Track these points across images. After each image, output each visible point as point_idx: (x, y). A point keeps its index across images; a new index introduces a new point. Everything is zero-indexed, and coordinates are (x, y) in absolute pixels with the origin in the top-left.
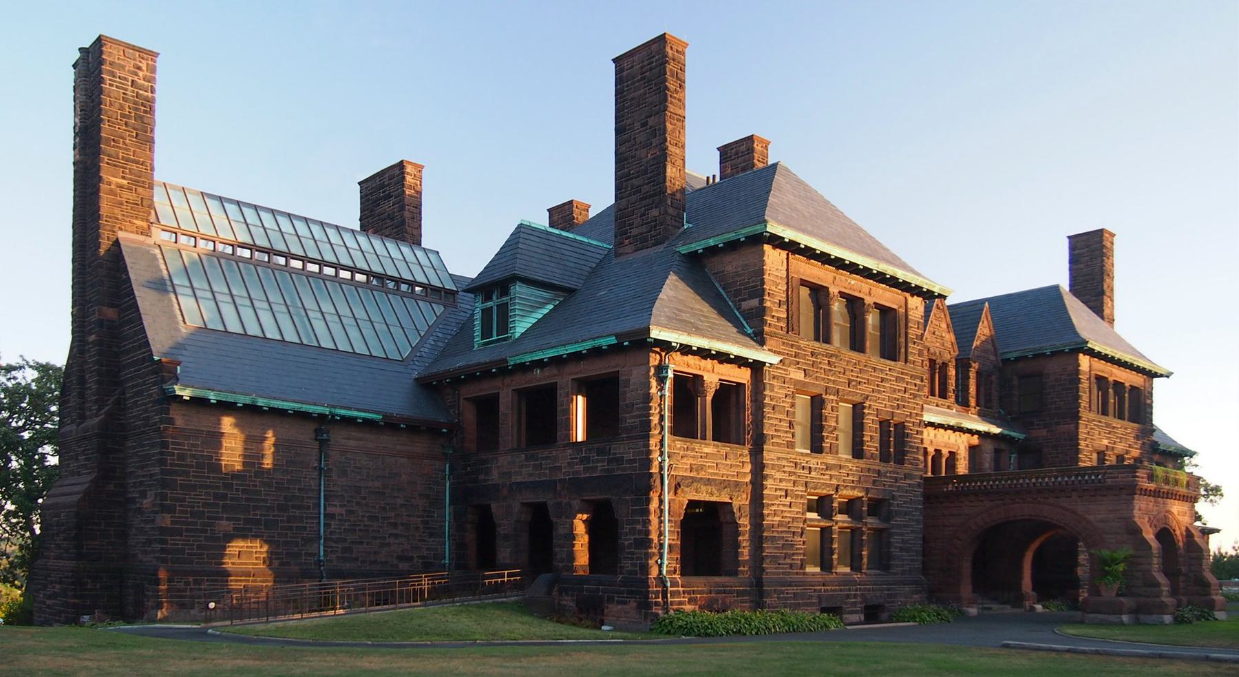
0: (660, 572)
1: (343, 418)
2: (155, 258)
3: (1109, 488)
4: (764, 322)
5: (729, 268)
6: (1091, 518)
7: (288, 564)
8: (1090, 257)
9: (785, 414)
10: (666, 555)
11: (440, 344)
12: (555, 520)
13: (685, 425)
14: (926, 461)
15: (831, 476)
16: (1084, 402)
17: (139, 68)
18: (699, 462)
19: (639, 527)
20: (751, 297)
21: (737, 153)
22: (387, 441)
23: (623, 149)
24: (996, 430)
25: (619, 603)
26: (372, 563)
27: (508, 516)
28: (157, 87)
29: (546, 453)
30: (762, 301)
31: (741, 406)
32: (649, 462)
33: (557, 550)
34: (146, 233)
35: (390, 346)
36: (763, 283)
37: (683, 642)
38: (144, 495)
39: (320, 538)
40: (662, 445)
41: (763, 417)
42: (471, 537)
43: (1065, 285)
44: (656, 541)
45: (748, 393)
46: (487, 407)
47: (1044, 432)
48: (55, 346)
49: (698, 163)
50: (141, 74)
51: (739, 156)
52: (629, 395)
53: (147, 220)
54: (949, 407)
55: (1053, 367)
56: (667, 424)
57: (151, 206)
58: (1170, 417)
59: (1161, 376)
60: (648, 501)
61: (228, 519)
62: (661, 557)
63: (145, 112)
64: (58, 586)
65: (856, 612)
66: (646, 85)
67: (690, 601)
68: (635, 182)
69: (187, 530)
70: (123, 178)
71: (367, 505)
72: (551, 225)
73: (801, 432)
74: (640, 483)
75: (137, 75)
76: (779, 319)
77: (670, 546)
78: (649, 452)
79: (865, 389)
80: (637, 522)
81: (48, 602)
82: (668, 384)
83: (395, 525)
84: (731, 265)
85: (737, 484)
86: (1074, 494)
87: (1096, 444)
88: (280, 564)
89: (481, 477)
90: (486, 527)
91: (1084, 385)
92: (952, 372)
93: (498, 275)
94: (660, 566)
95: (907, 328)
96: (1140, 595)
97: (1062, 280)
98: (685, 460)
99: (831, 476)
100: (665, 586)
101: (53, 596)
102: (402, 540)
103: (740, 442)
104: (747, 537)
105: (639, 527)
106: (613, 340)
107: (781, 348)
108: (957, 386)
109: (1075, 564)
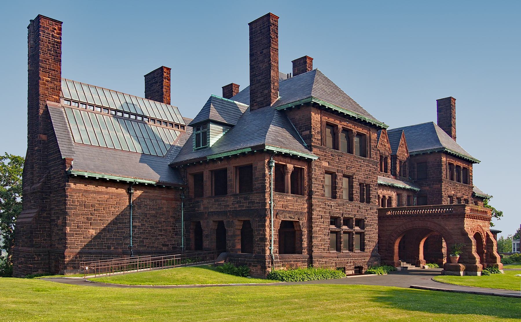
0: (270, 252)
1: (140, 183)
2: (62, 112)
3: (454, 215)
4: (311, 141)
5: (297, 117)
6: (447, 228)
7: (117, 248)
8: (446, 108)
9: (320, 183)
10: (272, 245)
11: (179, 149)
12: (226, 228)
13: (280, 188)
14: (379, 202)
15: (340, 209)
16: (444, 175)
17: (55, 29)
18: (286, 203)
19: (261, 232)
20: (306, 130)
21: (300, 64)
22: (156, 193)
23: (253, 63)
24: (408, 187)
25: (254, 266)
26: (152, 247)
27: (209, 227)
28: (62, 37)
29: (223, 199)
30: (311, 132)
31: (302, 179)
32: (265, 204)
33: (228, 242)
34: (58, 101)
35: (158, 151)
36: (311, 124)
37: (279, 284)
38: (58, 218)
39: (130, 236)
40: (270, 196)
41: (312, 183)
42: (192, 235)
43: (436, 123)
44: (268, 238)
45: (305, 172)
46: (199, 178)
47: (427, 188)
48: (21, 150)
49: (284, 68)
50: (55, 31)
51: (301, 65)
52: (257, 174)
53: (59, 96)
54: (388, 177)
55: (431, 159)
56: (272, 187)
57: (60, 90)
58: (480, 182)
59: (476, 163)
60: (265, 221)
61: (93, 229)
62: (271, 246)
63: (58, 48)
64: (23, 259)
65: (351, 270)
66: (263, 34)
67: (283, 265)
68: (258, 78)
69: (76, 234)
70: (49, 77)
71: (149, 221)
72: (224, 96)
73: (328, 192)
74: (261, 214)
75: (54, 32)
76: (318, 140)
77: (274, 241)
78: (265, 199)
79: (353, 170)
80: (261, 230)
81: (19, 266)
82: (273, 169)
83: (161, 231)
84: (298, 115)
85: (301, 213)
86: (440, 217)
87: (449, 193)
88: (114, 249)
89: (196, 209)
90: (199, 232)
91: (444, 167)
92: (389, 161)
93: (202, 119)
94: (270, 250)
95: (370, 142)
96: (468, 263)
97: (434, 119)
98: (280, 203)
99: (340, 209)
100: (272, 259)
101: (21, 263)
102: (164, 237)
103: (302, 194)
104: (306, 236)
105: (261, 232)
106: (250, 150)
107: (319, 152)
108: (391, 167)
109: (442, 247)
